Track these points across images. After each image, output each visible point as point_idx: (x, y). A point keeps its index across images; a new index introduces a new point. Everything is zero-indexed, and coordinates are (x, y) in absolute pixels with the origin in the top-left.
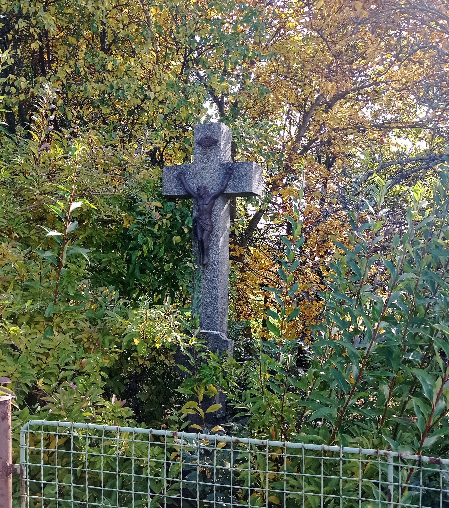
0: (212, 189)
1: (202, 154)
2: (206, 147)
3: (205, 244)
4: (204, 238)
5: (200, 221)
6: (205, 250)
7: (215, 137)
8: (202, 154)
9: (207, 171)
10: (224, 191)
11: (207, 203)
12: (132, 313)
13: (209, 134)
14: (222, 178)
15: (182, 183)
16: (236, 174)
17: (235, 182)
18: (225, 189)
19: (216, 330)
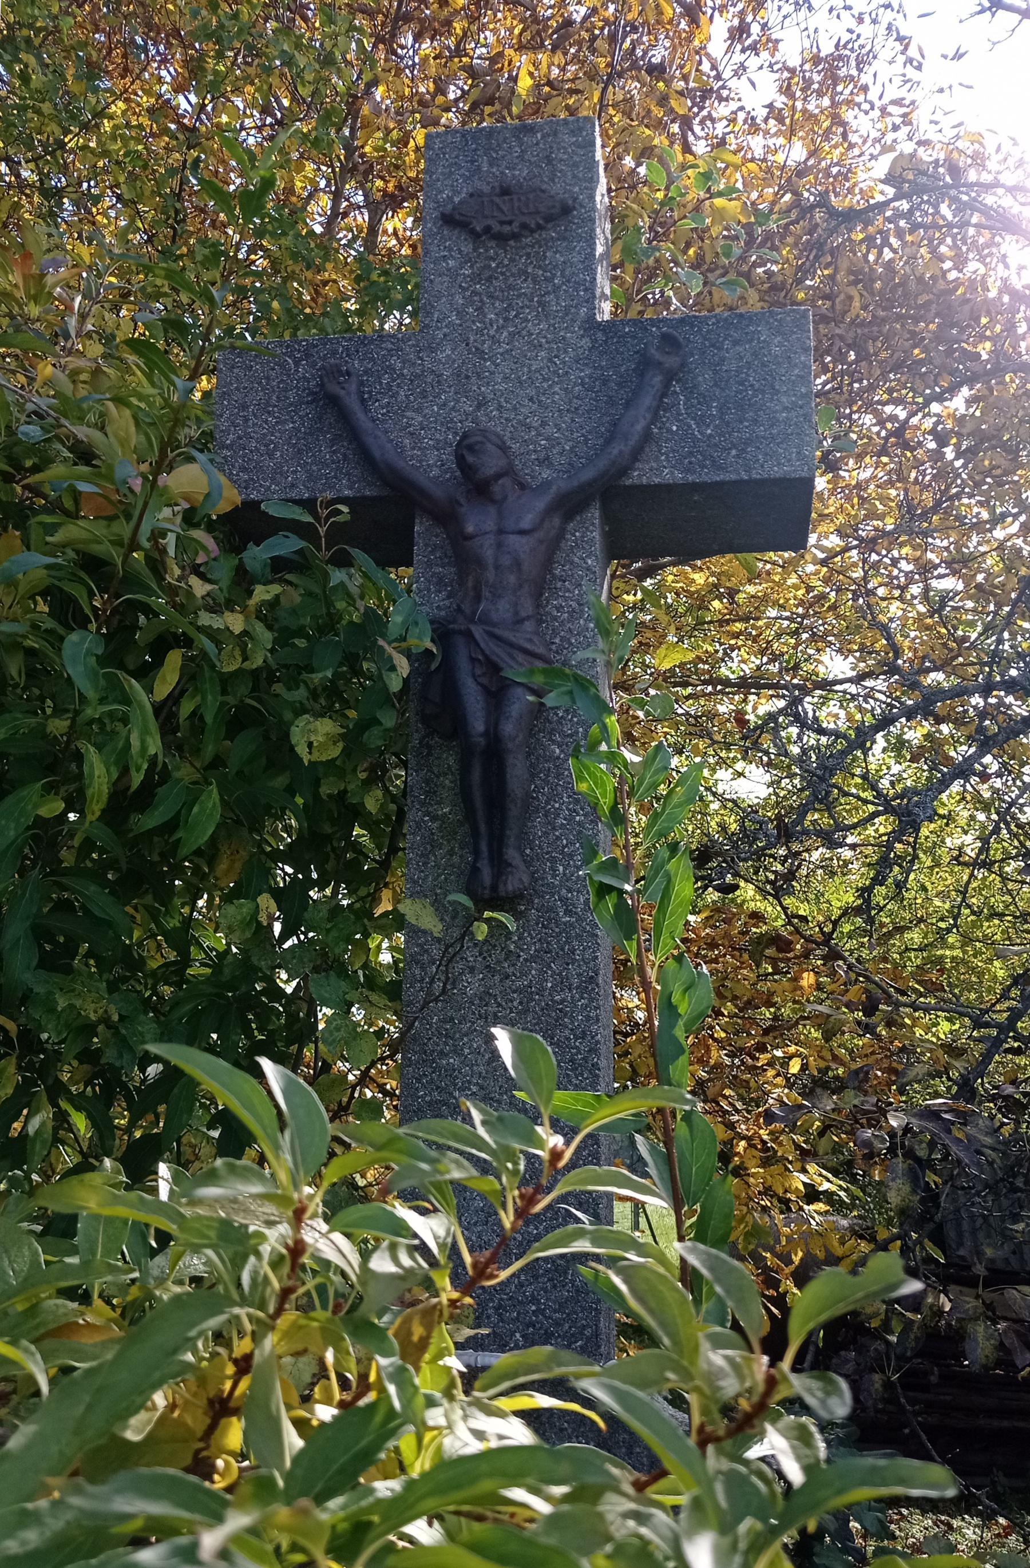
0: (545, 461)
1: (476, 278)
2: (501, 239)
3: (517, 769)
4: (508, 728)
5: (477, 631)
6: (514, 811)
7: (557, 189)
8: (476, 278)
9: (506, 367)
10: (624, 471)
11: (526, 523)
12: (846, 37)
13: (522, 172)
14: (611, 402)
15: (344, 417)
16: (704, 379)
17: (701, 421)
18: (636, 455)
19: (471, 1250)
